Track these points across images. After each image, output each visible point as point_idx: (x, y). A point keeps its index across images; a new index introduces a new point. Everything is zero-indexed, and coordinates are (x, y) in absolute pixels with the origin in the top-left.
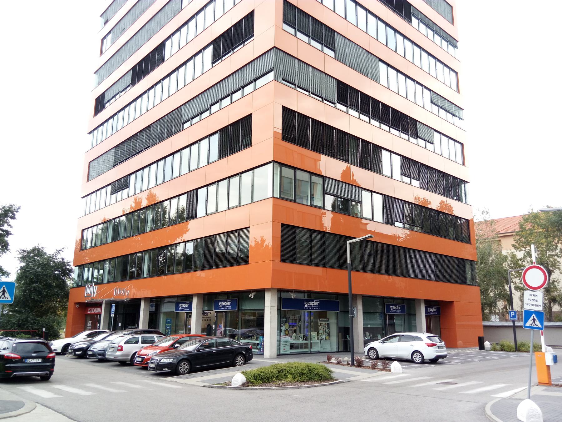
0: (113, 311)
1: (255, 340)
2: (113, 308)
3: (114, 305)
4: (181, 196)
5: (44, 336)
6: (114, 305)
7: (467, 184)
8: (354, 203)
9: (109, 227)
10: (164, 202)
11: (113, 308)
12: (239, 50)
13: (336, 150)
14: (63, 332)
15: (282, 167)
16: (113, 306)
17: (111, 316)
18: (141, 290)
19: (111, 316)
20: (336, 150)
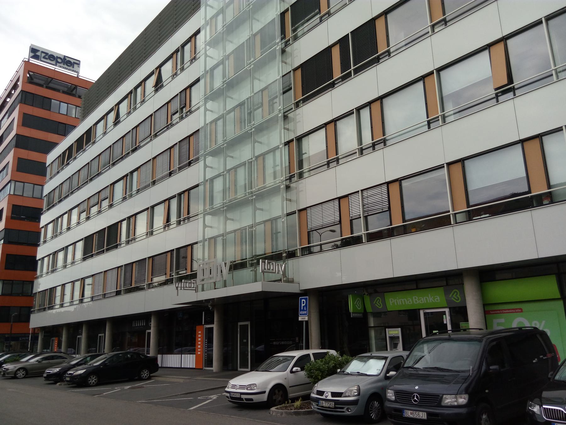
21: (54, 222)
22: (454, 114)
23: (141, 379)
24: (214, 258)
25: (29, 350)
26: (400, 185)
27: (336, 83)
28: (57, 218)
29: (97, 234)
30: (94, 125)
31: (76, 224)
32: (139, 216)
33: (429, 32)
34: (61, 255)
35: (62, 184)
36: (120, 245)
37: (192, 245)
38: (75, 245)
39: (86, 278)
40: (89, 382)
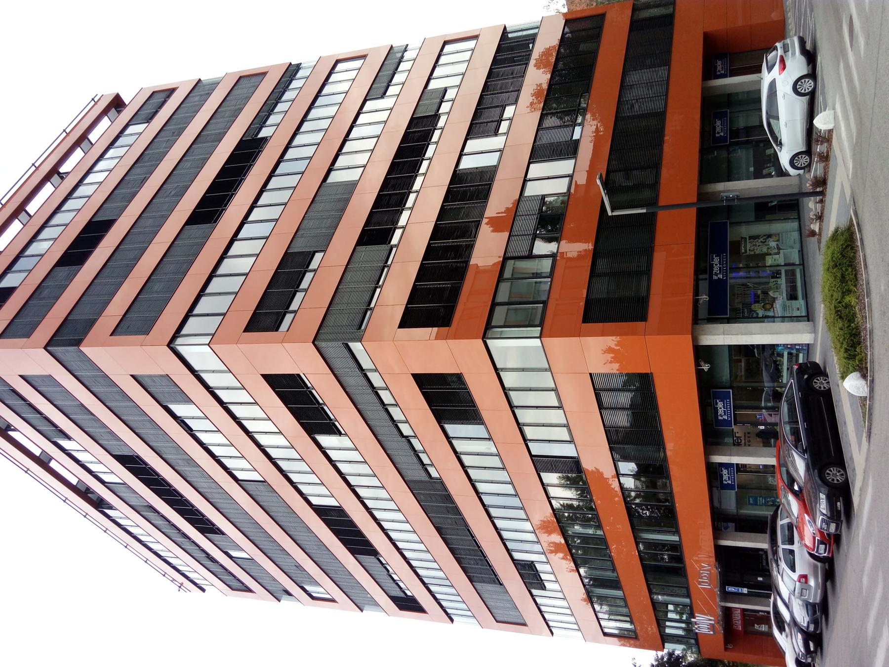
0: (738, 590)
2: (733, 590)
3: (728, 588)
6: (728, 588)
11: (733, 590)
16: (729, 589)
18: (700, 544)
19: (746, 592)
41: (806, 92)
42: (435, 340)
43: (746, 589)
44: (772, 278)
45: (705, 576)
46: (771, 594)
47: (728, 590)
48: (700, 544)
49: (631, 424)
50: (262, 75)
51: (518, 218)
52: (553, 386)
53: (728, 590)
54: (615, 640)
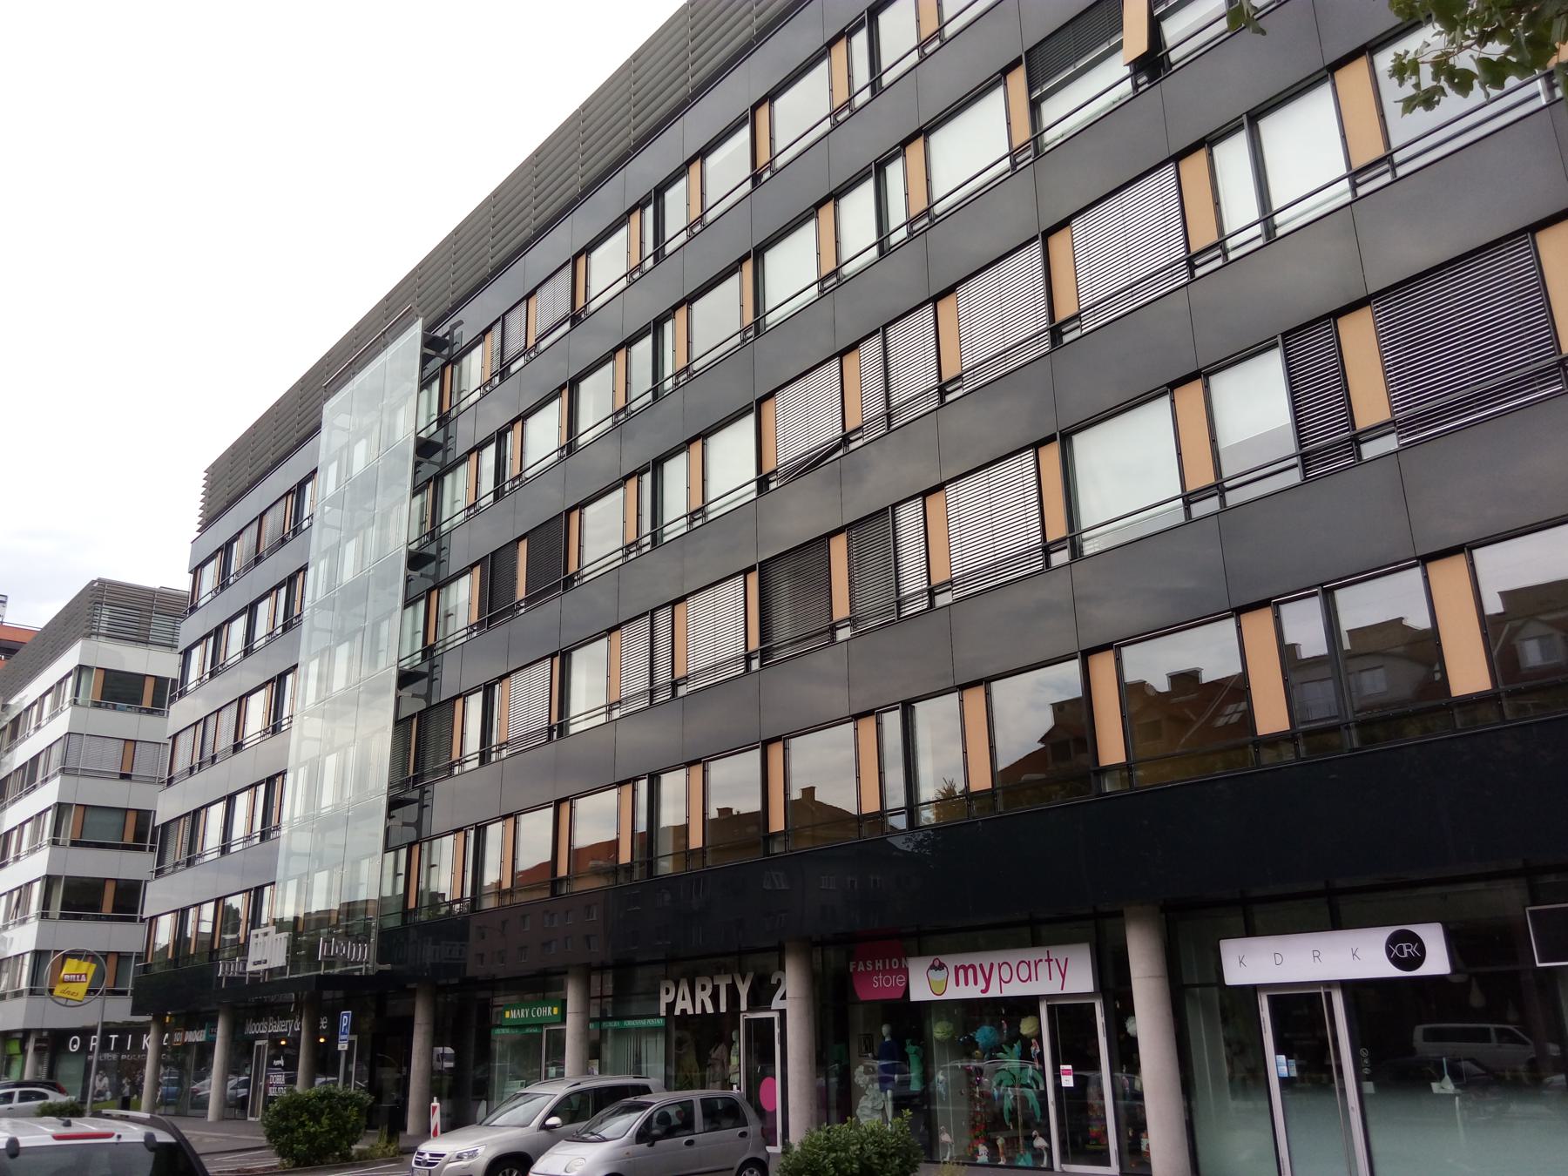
0: (344, 1033)
1: (134, 955)
2: (344, 1025)
3: (348, 1015)
4: (212, 807)
5: (331, 971)
6: (348, 1015)
7: (1442, 98)
8: (448, 338)
9: (1142, 788)
10: (993, 684)
11: (344, 1025)
12: (527, 329)
13: (38, 1045)
14: (301, 970)
15: (1275, 207)
16: (345, 1017)
17: (339, 1048)
18: (355, 1038)
19: (339, 1048)
20: (38, 1045)
21: (270, 685)
22: (791, 644)
23: (50, 1030)
24: (14, 941)
25: (1444, 1060)
26: (988, 695)
27: (948, 390)
28: (569, 511)
29: (187, 818)
30: (41, 697)
31: (259, 735)
32: (238, 797)
33: (1538, 95)
34: (216, 814)
35: (50, 746)
36: (461, 762)
37: (785, 739)
38: (256, 791)
39: (576, 798)
40: (851, 1147)
41: (989, 995)
42: (1279, 1077)
43: (346, 1048)
44: (192, 1108)
45: (341, 950)
46: (1133, 694)
47: (345, 1014)
48: (355, 1038)
49: (490, 1031)
50: (27, 762)
51: (168, 1113)
52: (1075, 665)
53: (345, 1014)
54: (1193, 1103)
